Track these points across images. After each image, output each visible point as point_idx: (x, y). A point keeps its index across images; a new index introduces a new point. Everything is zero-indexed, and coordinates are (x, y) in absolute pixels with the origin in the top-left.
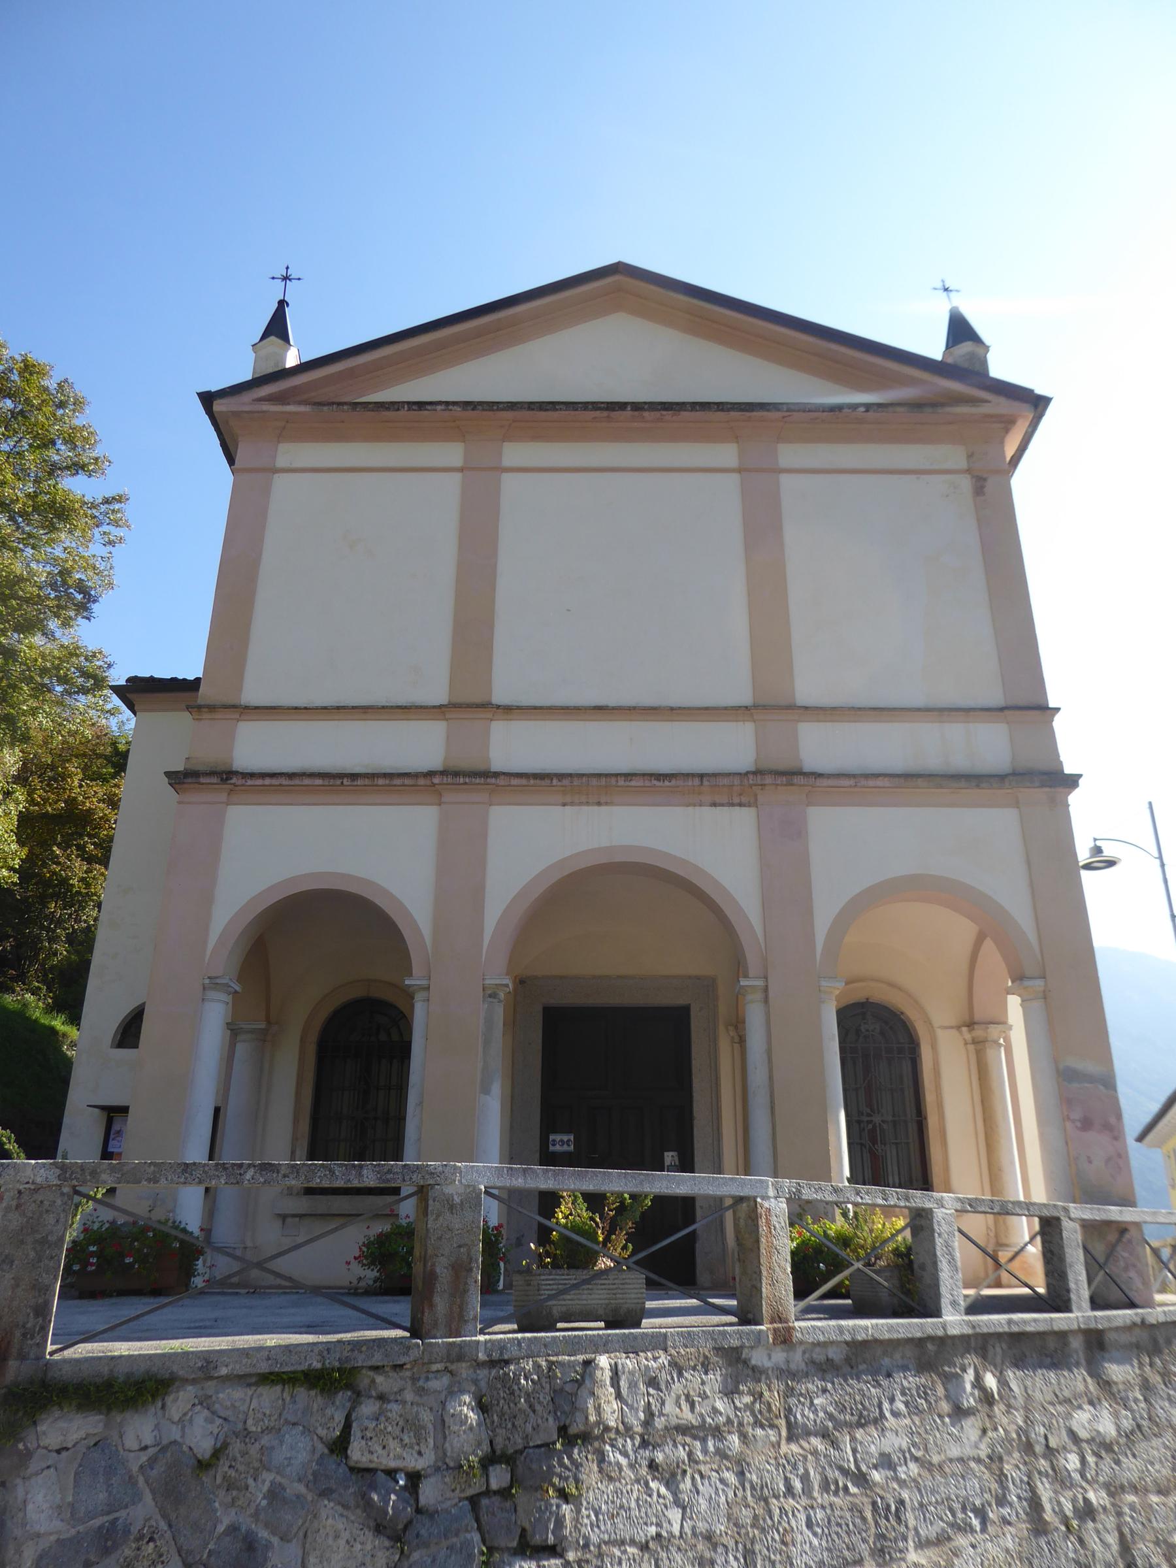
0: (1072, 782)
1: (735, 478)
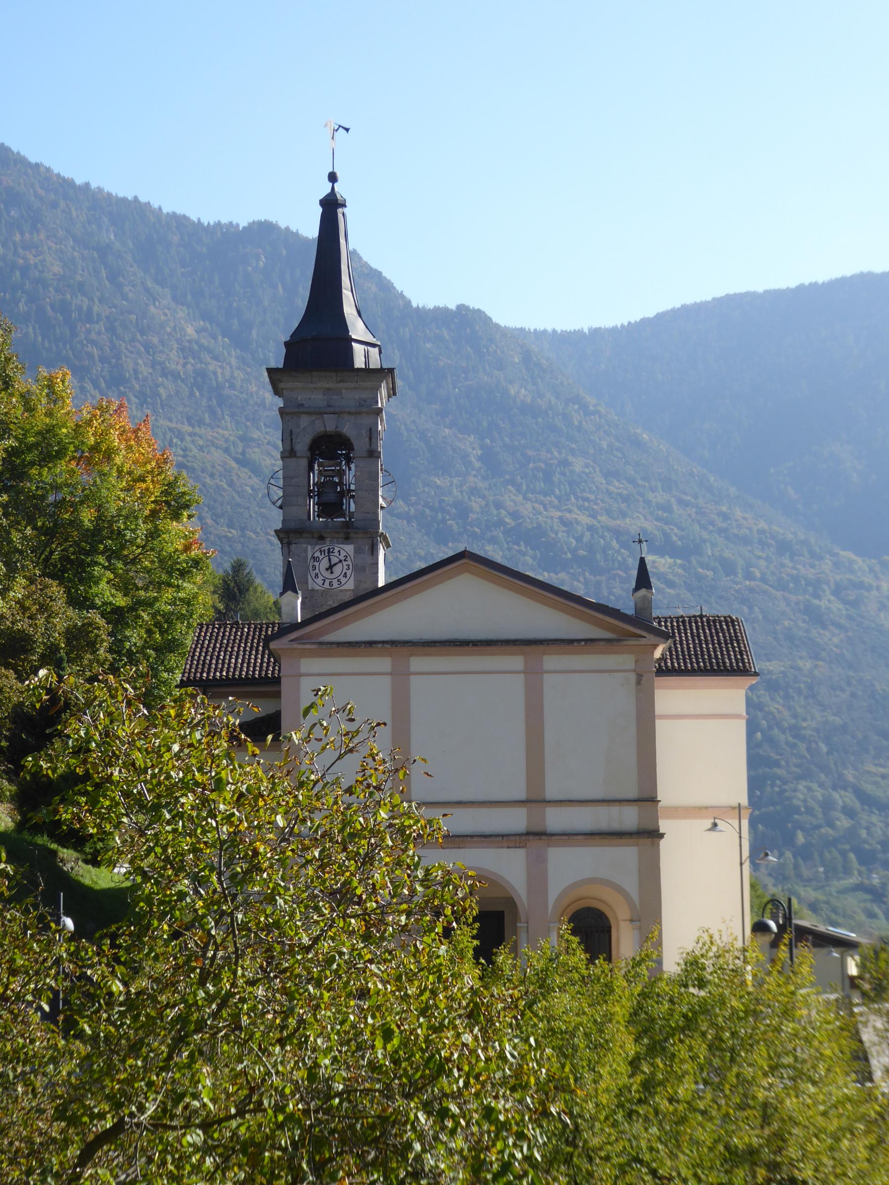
0: (662, 836)
1: (522, 676)
